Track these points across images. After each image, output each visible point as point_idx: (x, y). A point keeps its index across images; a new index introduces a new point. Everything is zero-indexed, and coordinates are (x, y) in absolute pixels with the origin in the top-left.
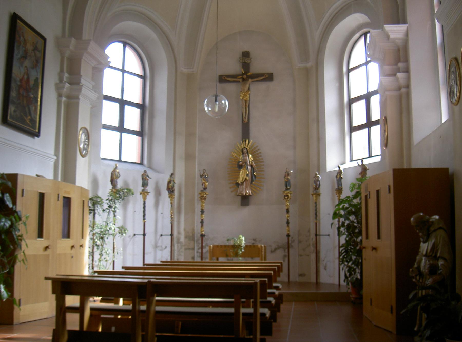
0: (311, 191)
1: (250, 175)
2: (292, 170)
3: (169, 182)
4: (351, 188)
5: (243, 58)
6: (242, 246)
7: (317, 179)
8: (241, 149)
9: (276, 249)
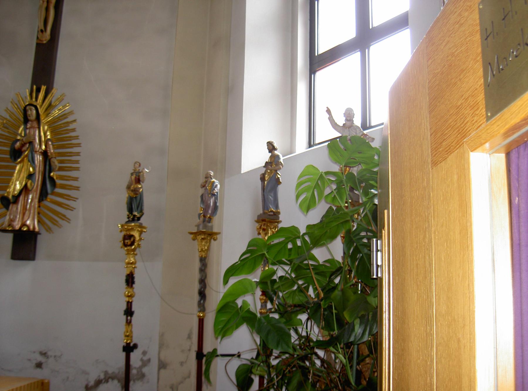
1: (38, 178)
2: (150, 167)
4: (306, 190)
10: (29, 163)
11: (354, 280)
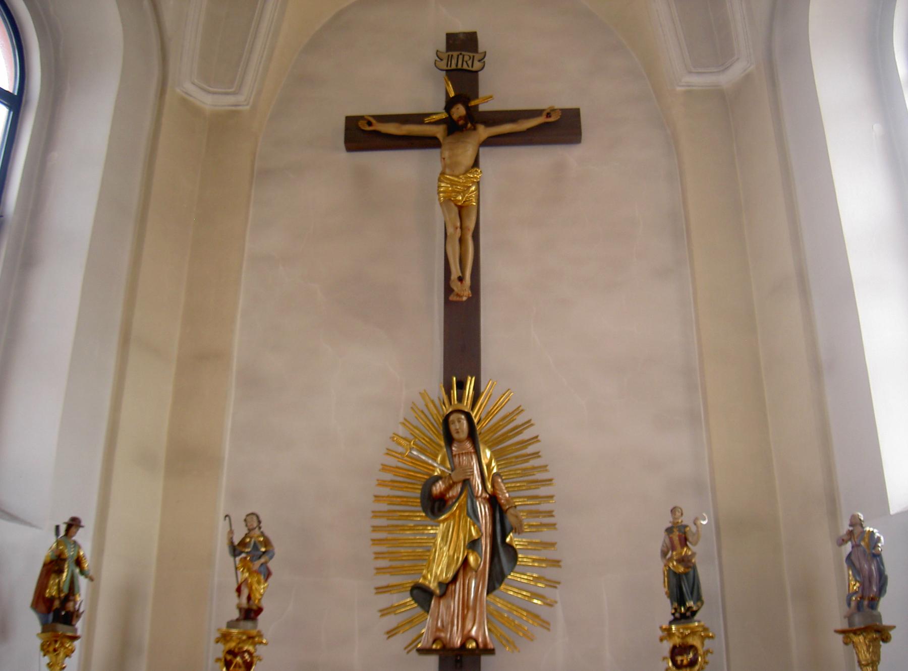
1: (485, 544)
3: (54, 566)
5: (450, 53)
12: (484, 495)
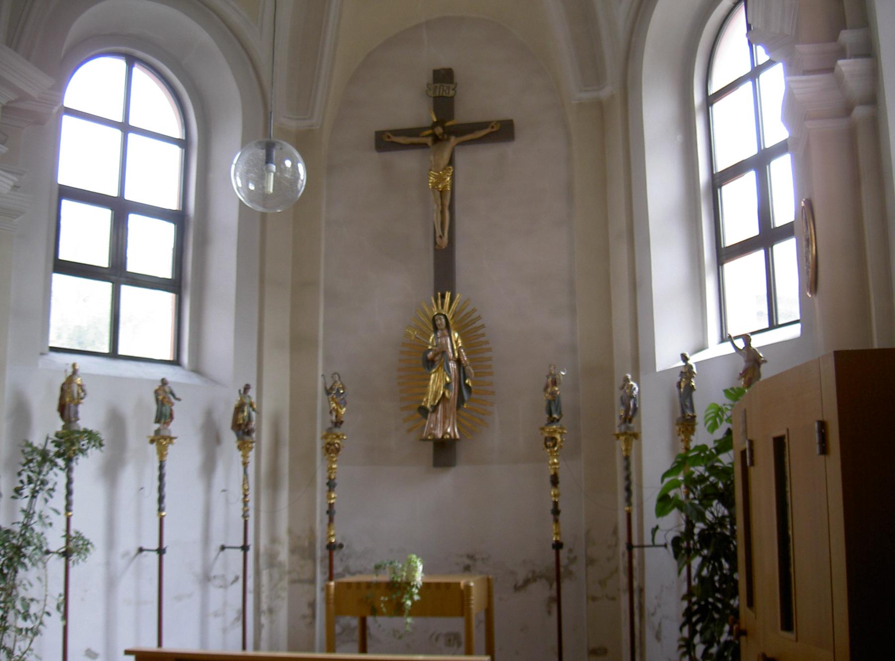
0: (617, 426)
1: (454, 386)
2: (565, 370)
3: (239, 409)
5: (435, 85)
6: (413, 586)
7: (627, 391)
8: (431, 317)
9: (527, 582)
10: (445, 373)
11: (700, 485)
12: (454, 359)
